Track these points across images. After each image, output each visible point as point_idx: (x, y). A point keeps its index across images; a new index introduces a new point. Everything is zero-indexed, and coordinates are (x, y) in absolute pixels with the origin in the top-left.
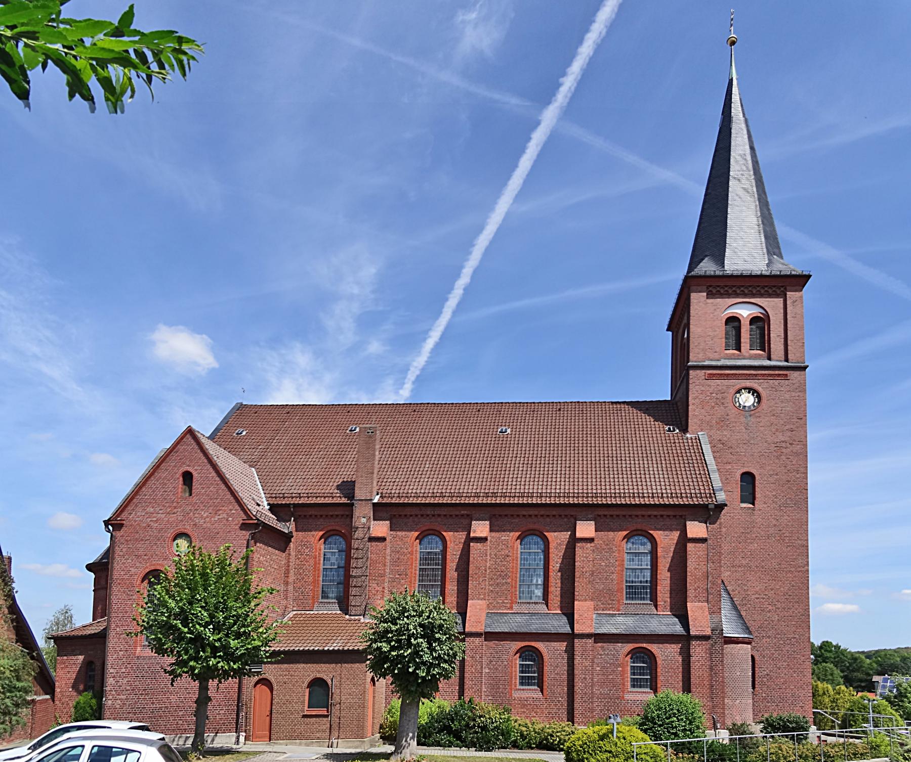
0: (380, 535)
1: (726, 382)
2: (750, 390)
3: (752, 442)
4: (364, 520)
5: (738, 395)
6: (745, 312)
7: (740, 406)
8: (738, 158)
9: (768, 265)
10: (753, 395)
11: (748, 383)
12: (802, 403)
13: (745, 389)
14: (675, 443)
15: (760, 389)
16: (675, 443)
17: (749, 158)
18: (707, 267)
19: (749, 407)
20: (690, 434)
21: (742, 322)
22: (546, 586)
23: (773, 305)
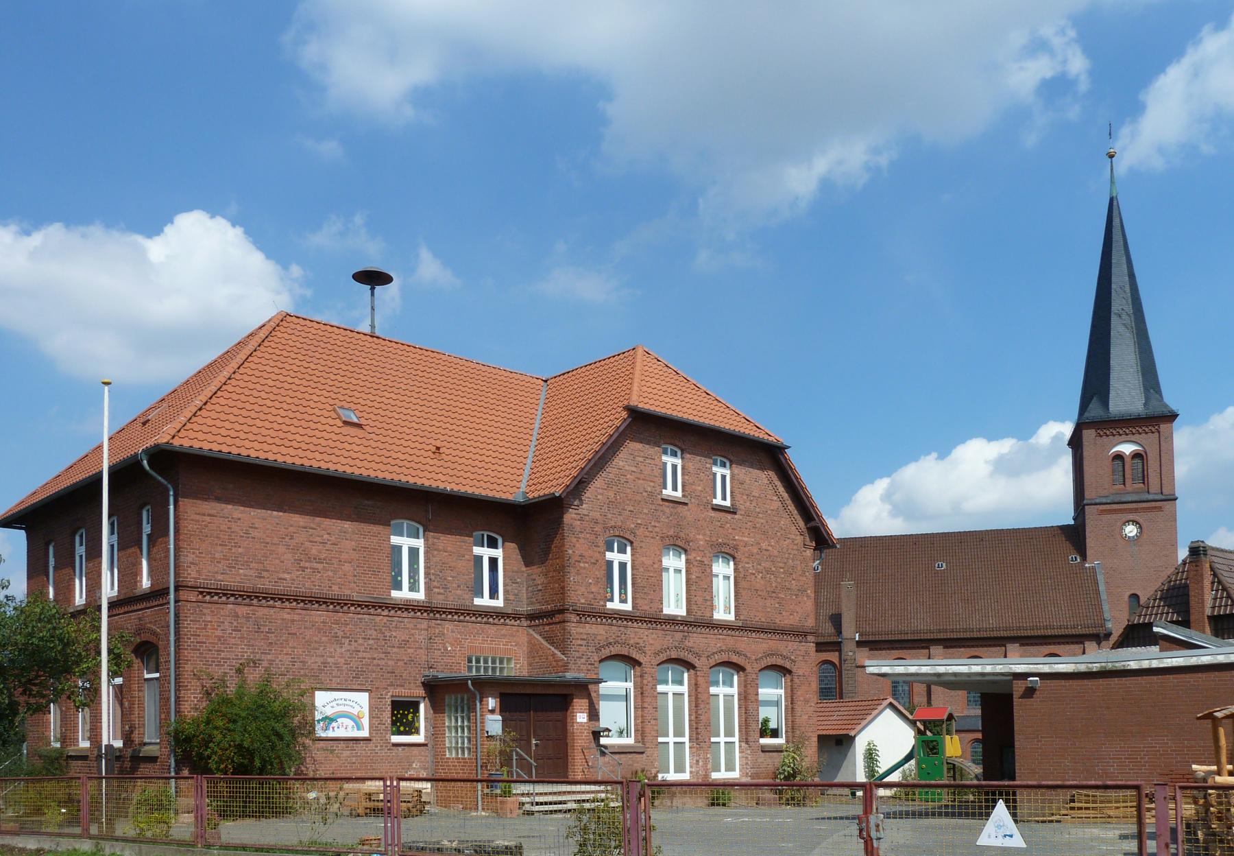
0: (962, 649)
1: (1114, 516)
2: (1135, 522)
3: (1136, 568)
4: (850, 654)
5: (1124, 527)
6: (1127, 449)
7: (1126, 537)
8: (1118, 289)
9: (1145, 405)
10: (1133, 524)
11: (1131, 517)
12: (875, 539)
13: (1133, 521)
14: (1076, 573)
15: (1141, 521)
16: (1076, 573)
17: (1128, 289)
18: (1095, 411)
19: (1133, 537)
20: (1089, 564)
21: (1125, 459)
22: (308, 852)
23: (1150, 440)
